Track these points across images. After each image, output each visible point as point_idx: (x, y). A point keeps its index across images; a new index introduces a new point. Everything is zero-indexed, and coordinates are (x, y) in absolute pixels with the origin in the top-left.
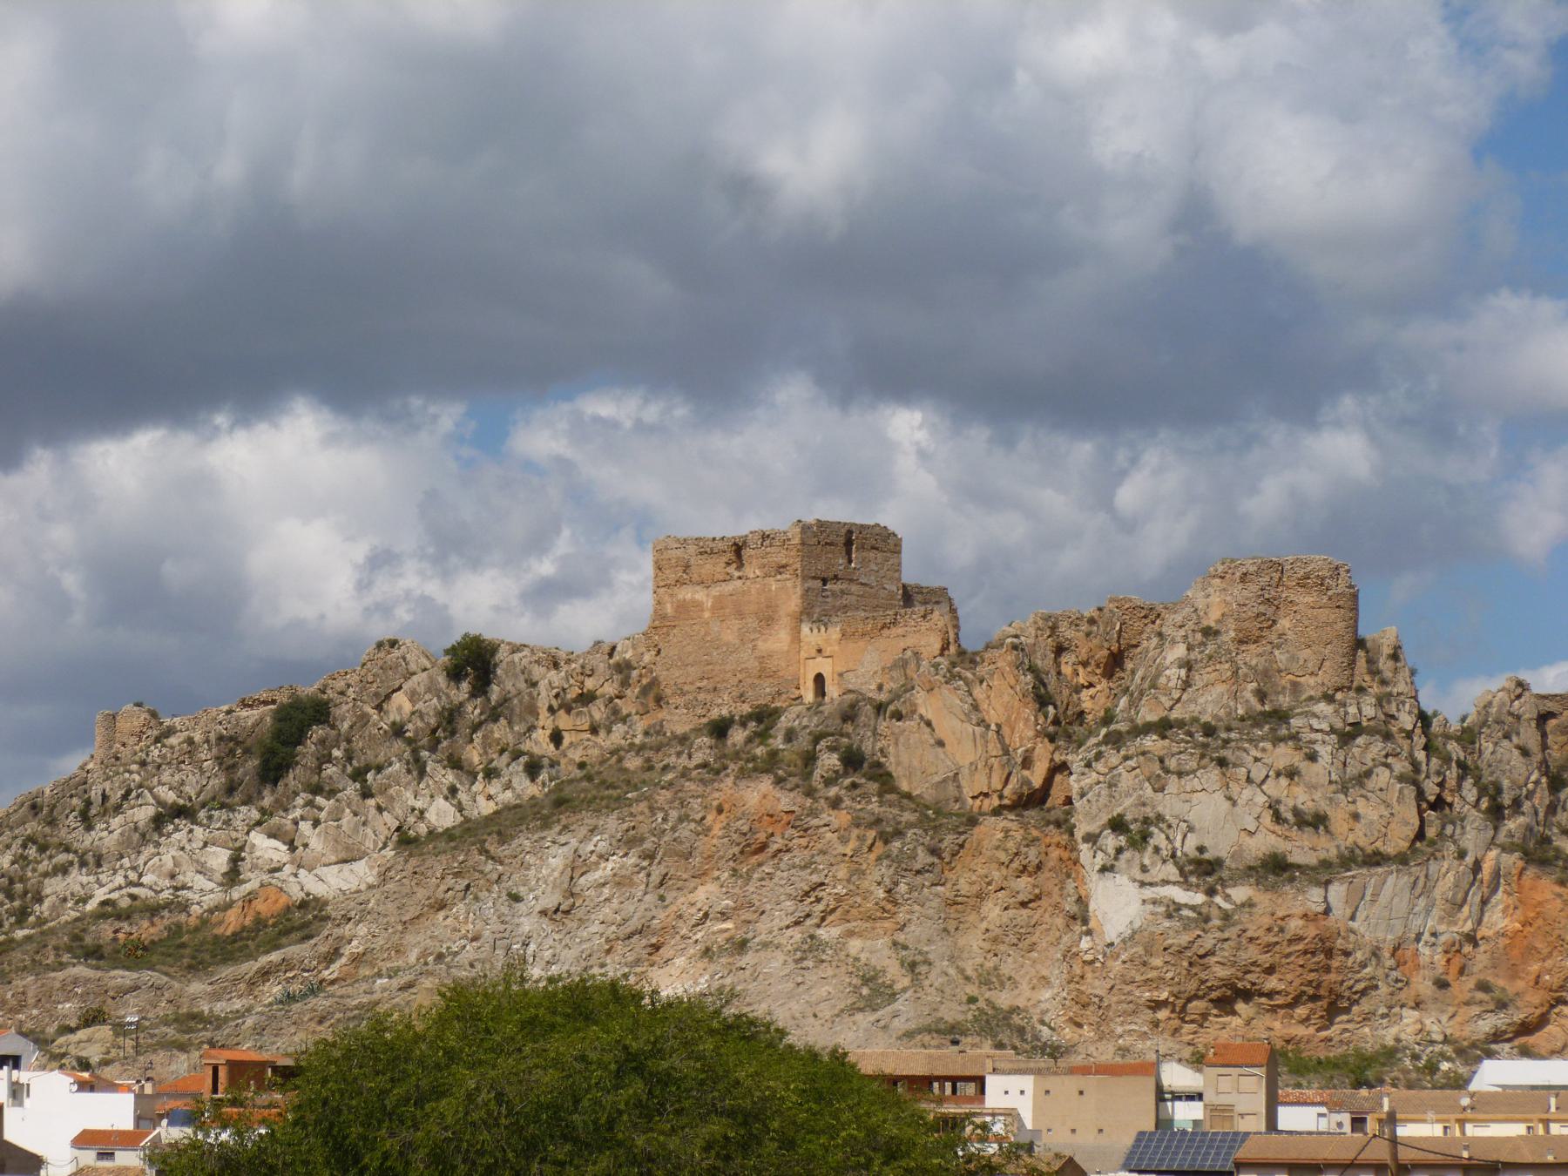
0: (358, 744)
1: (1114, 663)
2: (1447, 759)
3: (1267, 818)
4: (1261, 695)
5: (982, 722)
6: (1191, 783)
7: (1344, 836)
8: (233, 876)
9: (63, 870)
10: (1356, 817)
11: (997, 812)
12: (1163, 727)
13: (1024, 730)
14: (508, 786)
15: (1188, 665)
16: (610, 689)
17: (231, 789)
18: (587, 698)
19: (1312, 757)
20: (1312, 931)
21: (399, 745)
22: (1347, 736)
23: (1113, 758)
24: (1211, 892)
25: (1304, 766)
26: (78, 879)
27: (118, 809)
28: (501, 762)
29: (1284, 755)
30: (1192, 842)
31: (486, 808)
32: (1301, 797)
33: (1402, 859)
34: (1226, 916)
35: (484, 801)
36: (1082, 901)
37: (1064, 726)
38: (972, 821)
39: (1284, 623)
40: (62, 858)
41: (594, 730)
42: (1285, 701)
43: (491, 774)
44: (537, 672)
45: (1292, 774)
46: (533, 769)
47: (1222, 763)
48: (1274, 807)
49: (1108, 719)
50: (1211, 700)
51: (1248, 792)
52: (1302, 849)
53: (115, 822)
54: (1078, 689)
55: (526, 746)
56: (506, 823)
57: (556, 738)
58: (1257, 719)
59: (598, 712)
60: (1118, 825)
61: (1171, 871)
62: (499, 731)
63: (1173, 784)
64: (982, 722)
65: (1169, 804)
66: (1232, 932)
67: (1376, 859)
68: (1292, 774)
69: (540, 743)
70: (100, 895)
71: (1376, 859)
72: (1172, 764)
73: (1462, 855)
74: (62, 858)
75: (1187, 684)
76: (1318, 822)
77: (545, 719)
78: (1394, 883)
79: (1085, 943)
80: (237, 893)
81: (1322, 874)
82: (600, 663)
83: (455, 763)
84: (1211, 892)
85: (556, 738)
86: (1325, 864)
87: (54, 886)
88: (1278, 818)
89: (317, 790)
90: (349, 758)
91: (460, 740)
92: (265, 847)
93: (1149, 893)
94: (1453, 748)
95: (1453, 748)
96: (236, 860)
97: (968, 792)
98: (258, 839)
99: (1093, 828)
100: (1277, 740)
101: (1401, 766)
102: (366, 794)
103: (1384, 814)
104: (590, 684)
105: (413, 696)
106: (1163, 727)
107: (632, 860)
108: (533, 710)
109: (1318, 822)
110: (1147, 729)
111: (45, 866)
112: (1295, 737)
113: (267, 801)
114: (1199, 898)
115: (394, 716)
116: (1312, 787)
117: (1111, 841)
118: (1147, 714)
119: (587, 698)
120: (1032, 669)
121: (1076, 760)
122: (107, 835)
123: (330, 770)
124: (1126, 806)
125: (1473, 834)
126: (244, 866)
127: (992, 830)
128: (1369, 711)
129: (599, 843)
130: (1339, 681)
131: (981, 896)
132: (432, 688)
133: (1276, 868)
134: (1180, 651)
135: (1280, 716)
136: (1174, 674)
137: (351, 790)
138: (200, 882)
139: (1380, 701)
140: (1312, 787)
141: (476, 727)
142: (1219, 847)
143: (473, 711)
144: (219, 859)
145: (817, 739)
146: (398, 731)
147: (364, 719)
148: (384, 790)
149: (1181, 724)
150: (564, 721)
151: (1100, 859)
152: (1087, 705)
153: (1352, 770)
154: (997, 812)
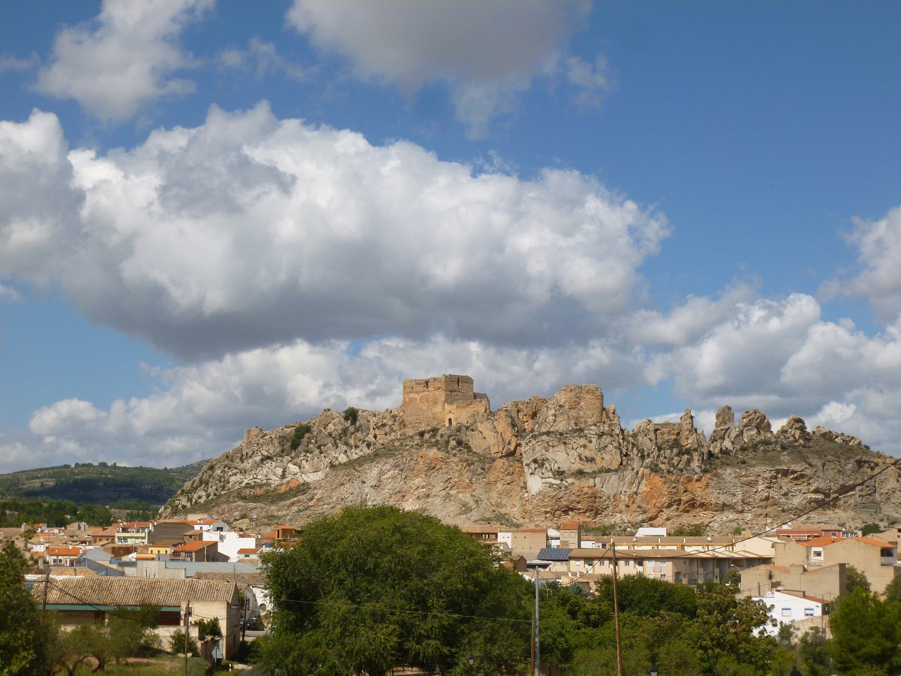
0: (319, 438)
1: (534, 415)
2: (629, 442)
3: (578, 459)
4: (576, 424)
5: (496, 432)
6: (556, 449)
7: (600, 464)
8: (283, 476)
9: (235, 474)
10: (603, 459)
11: (501, 457)
12: (548, 433)
13: (509, 434)
14: (361, 450)
15: (555, 416)
16: (390, 423)
17: (283, 451)
18: (384, 425)
19: (590, 442)
20: (591, 491)
21: (330, 439)
22: (600, 436)
23: (534, 442)
24: (562, 480)
25: (588, 444)
26: (239, 477)
27: (251, 457)
28: (359, 443)
29: (582, 441)
30: (556, 466)
31: (355, 457)
32: (587, 453)
33: (616, 471)
34: (566, 487)
35: (355, 455)
36: (525, 483)
37: (520, 433)
38: (494, 460)
39: (582, 404)
40: (235, 471)
41: (386, 434)
42: (583, 426)
43: (356, 447)
44: (370, 418)
45: (585, 446)
46: (368, 446)
47: (565, 443)
48: (580, 456)
49: (532, 431)
50: (561, 426)
51: (572, 452)
52: (588, 468)
53: (250, 461)
54: (524, 422)
55: (367, 439)
56: (361, 461)
57: (375, 437)
58: (575, 431)
59: (387, 429)
60: (535, 461)
61: (551, 474)
62: (359, 435)
63: (551, 449)
64: (496, 432)
65: (550, 455)
66: (568, 492)
67: (608, 471)
68: (585, 446)
69: (370, 438)
70: (246, 481)
71: (608, 471)
72: (551, 444)
73: (633, 469)
74: (235, 471)
75: (555, 421)
76: (592, 460)
77: (372, 431)
78: (614, 477)
79: (526, 495)
80: (285, 481)
81: (594, 474)
82: (388, 415)
83: (346, 444)
84: (562, 480)
85: (375, 437)
86: (594, 472)
87: (233, 479)
88: (581, 459)
89: (307, 451)
90: (316, 442)
91: (348, 437)
92: (292, 468)
93: (544, 480)
94: (630, 438)
95: (630, 438)
96: (284, 471)
97: (492, 452)
98: (290, 465)
99: (528, 462)
100: (580, 437)
101: (616, 444)
102: (321, 453)
103: (611, 458)
104: (385, 421)
105: (334, 425)
106: (548, 433)
107: (397, 471)
108: (369, 429)
109: (592, 460)
110: (544, 434)
111: (230, 473)
112: (585, 436)
113: (293, 455)
114: (558, 482)
115: (329, 431)
116: (590, 450)
117: (533, 466)
118: (544, 430)
119: (384, 425)
120: (511, 417)
121: (523, 443)
122: (248, 464)
123: (311, 446)
124: (537, 456)
125: (636, 464)
126: (287, 473)
127: (499, 463)
128: (606, 428)
129: (388, 467)
130: (597, 420)
131: (496, 482)
132: (340, 422)
133: (580, 473)
134: (553, 411)
135: (581, 430)
136: (551, 418)
137: (317, 451)
138: (274, 478)
139: (610, 426)
140: (590, 450)
141: (352, 434)
142: (564, 468)
143: (352, 429)
144: (279, 471)
145: (449, 437)
146: (330, 435)
147: (321, 431)
148: (326, 452)
149: (553, 432)
150: (377, 432)
151: (530, 471)
152: (526, 427)
153: (602, 445)
154: (501, 457)
